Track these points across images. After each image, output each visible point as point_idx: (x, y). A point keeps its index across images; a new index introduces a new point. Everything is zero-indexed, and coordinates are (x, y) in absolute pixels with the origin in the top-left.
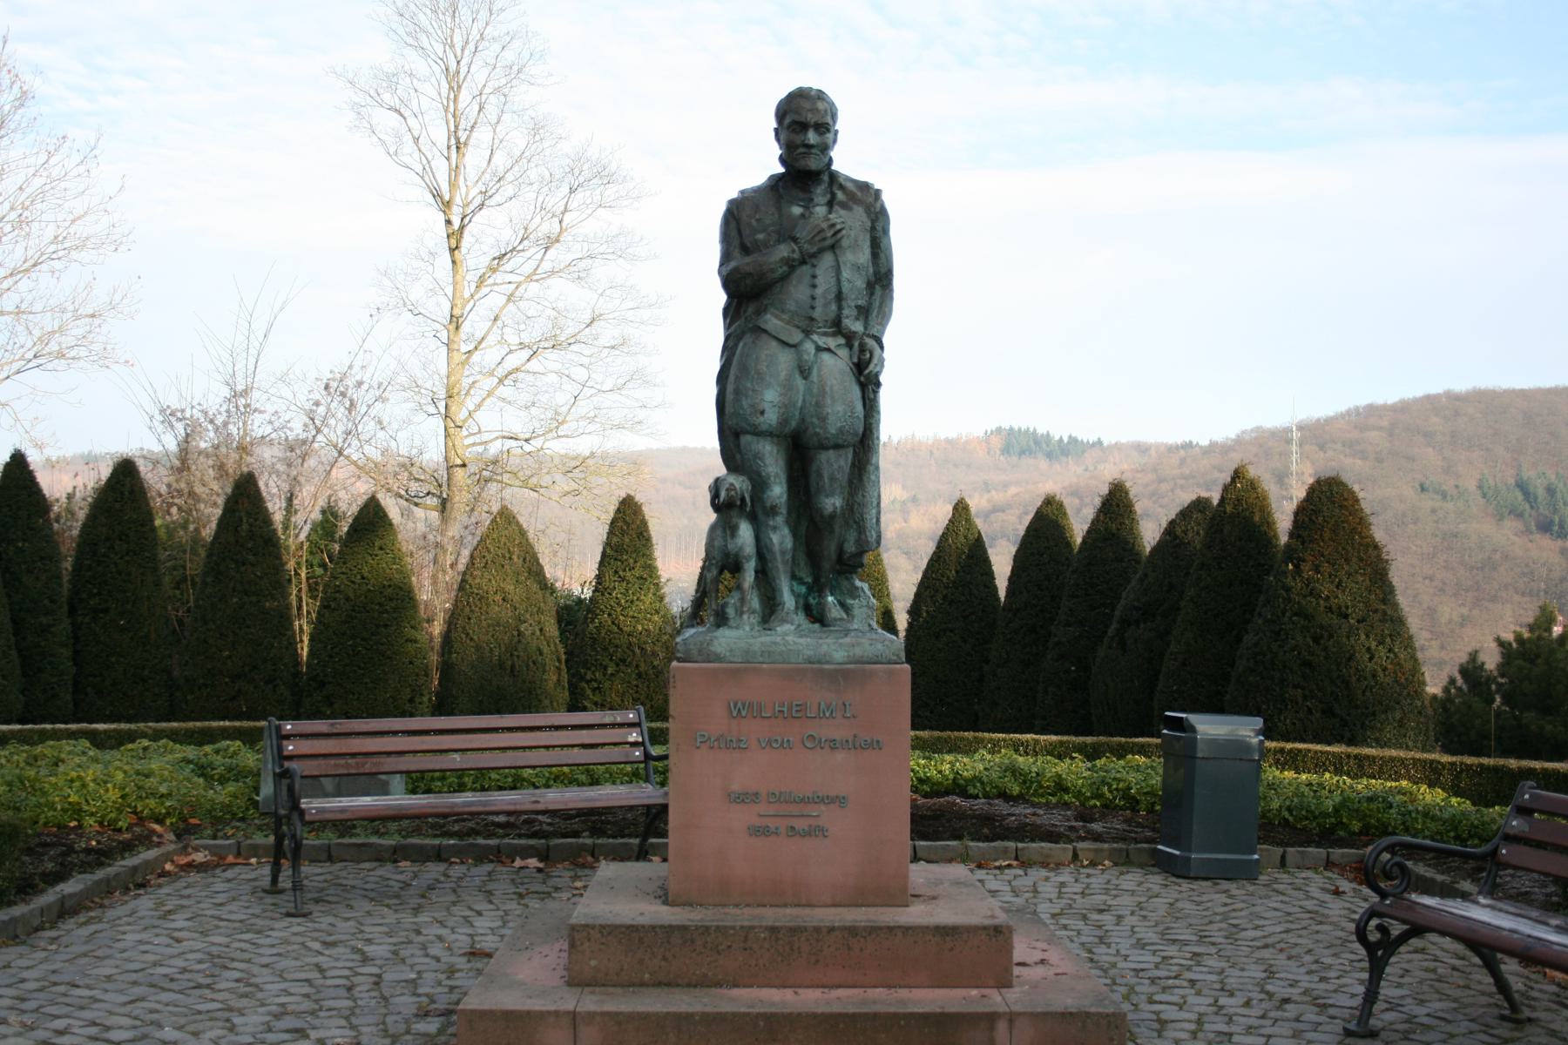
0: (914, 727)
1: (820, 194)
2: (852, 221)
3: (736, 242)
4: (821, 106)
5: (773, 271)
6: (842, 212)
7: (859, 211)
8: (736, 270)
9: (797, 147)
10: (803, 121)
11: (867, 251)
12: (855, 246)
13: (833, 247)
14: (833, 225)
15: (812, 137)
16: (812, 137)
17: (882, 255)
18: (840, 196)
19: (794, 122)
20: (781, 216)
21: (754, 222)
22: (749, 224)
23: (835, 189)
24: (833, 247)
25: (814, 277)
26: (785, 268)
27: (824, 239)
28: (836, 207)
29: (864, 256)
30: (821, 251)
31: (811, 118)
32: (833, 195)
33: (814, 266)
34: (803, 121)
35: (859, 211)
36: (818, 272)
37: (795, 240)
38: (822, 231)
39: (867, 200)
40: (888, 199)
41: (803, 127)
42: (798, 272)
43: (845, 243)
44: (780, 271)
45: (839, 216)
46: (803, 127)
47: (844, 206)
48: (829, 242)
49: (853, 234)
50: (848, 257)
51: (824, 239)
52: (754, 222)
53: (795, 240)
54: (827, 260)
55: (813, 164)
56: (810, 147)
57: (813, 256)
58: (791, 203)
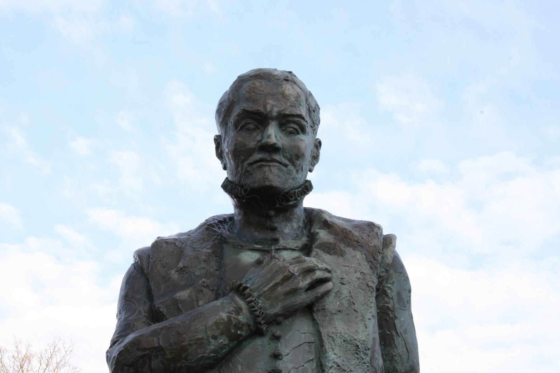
0: (194, 308)
1: (289, 231)
2: (347, 273)
3: (143, 308)
4: (288, 89)
5: (200, 343)
6: (327, 257)
7: (356, 257)
8: (134, 343)
9: (251, 152)
10: (264, 126)
11: (372, 324)
12: (349, 311)
13: (309, 309)
14: (310, 270)
15: (273, 134)
16: (273, 134)
17: (398, 341)
18: (323, 235)
19: (246, 114)
20: (220, 266)
21: (174, 275)
22: (166, 279)
23: (316, 229)
24: (309, 309)
25: (276, 356)
26: (223, 340)
27: (294, 291)
28: (315, 251)
29: (368, 331)
30: (290, 313)
31: (273, 107)
32: (312, 237)
33: (277, 338)
34: (264, 126)
35: (356, 257)
36: (283, 349)
37: (240, 290)
38: (289, 277)
39: (373, 249)
40: (404, 251)
41: (260, 120)
42: (248, 349)
43: (331, 304)
44: (213, 345)
45: (320, 261)
46: (260, 120)
47: (329, 248)
48: (303, 298)
49: (345, 291)
50: (337, 328)
51: (294, 291)
52: (174, 275)
53: (240, 290)
54: (300, 331)
55: (275, 177)
56: (274, 149)
57: (274, 321)
58: (241, 248)
